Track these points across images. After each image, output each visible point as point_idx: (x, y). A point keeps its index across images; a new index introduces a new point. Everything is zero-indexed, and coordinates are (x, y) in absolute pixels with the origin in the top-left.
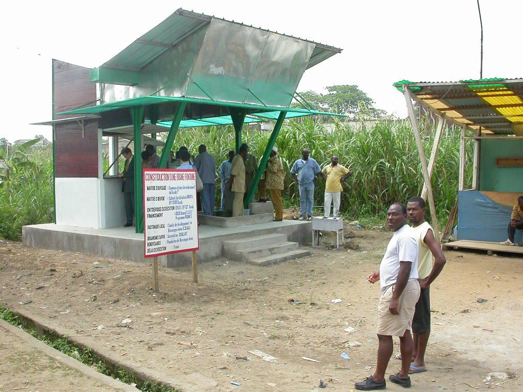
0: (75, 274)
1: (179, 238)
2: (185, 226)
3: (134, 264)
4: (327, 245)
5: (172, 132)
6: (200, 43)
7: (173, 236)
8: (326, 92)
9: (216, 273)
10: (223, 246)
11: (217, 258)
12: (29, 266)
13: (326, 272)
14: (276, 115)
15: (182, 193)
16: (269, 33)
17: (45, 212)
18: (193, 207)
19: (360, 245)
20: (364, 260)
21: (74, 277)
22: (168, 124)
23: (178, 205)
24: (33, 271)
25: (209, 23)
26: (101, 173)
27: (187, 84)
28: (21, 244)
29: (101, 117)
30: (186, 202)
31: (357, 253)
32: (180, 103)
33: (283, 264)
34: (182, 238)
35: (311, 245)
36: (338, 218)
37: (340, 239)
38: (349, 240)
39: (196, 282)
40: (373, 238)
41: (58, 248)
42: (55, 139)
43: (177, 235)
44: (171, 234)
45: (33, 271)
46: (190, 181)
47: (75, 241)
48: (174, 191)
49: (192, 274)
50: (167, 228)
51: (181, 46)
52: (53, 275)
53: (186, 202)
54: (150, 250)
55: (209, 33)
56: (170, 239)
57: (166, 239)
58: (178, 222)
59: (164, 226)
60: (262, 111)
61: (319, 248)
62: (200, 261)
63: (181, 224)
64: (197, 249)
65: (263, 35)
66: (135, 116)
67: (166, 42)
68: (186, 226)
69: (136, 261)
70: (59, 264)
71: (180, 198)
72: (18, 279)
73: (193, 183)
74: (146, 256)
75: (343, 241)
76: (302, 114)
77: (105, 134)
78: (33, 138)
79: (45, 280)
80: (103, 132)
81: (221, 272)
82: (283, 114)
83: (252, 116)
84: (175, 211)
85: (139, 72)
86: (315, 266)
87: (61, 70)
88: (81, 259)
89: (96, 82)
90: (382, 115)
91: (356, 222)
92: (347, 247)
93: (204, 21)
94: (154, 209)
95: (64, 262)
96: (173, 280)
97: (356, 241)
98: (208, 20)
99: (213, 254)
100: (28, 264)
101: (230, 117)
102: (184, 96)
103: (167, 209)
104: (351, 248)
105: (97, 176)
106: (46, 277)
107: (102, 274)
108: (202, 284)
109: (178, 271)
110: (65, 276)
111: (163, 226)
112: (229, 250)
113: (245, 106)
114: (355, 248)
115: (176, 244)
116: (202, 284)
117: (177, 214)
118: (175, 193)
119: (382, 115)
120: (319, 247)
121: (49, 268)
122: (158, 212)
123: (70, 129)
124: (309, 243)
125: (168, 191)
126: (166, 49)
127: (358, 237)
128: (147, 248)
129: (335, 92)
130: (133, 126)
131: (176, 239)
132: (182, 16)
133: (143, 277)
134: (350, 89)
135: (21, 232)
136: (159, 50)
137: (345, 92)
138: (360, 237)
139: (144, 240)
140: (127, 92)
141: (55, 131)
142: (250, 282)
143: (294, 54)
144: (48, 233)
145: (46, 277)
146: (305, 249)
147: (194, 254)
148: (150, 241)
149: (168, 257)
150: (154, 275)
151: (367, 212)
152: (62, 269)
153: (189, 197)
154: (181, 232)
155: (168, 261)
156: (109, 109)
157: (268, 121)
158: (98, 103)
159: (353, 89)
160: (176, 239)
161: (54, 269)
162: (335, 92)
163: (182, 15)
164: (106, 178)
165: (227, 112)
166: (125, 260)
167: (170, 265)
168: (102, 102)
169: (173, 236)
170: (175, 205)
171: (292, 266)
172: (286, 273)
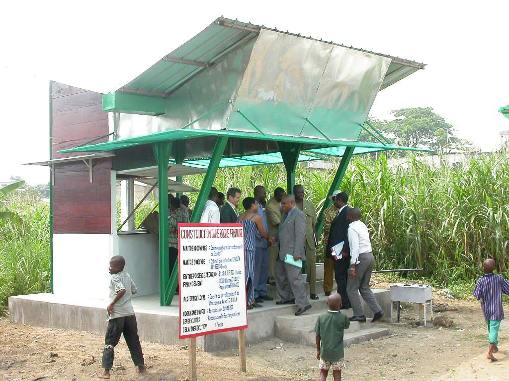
0: (84, 360)
1: (222, 312)
2: (230, 297)
3: (160, 346)
4: (410, 321)
5: (211, 172)
6: (246, 61)
7: (215, 310)
8: (391, 118)
9: (268, 358)
10: (275, 323)
11: (268, 338)
12: (22, 349)
13: (413, 357)
14: (341, 151)
15: (227, 254)
16: (332, 45)
17: (37, 278)
18: (240, 272)
19: (454, 320)
20: (462, 342)
21: (83, 365)
22: (204, 164)
23: (222, 270)
24: (28, 356)
25: (258, 34)
26: (114, 229)
27: (228, 113)
28: (7, 320)
29: (115, 155)
30: (231, 266)
31: (452, 332)
32: (220, 137)
33: (354, 347)
34: (227, 312)
35: (388, 322)
36: (424, 286)
37: (428, 312)
38: (439, 314)
39: (244, 370)
40: (471, 311)
41: (56, 325)
42: (53, 184)
43: (220, 310)
44: (213, 307)
45: (28, 356)
46: (236, 238)
47: (79, 316)
48: (216, 251)
49: (238, 360)
50: (207, 300)
51: (221, 64)
52: (54, 361)
53: (231, 266)
54: (187, 328)
55: (259, 47)
56: (212, 315)
57: (207, 314)
58: (221, 292)
59: (204, 296)
60: (321, 146)
61: (400, 326)
62: (247, 344)
63: (225, 296)
64: (246, 327)
65: (325, 49)
66: (159, 153)
67: (202, 59)
68: (232, 297)
69: (162, 343)
70: (61, 347)
71: (224, 260)
72: (9, 367)
73: (240, 241)
74: (182, 337)
75: (433, 316)
76: (377, 149)
77: (120, 177)
78: (9, 182)
79: (44, 368)
80: (117, 175)
81: (274, 358)
82: (349, 150)
83: (307, 153)
84: (218, 277)
85: (165, 98)
86: (397, 350)
87: (61, 94)
88: (89, 340)
89: (109, 111)
90: (467, 146)
91: (447, 290)
92: (438, 323)
93: (251, 32)
94: (191, 276)
95: (67, 344)
96: (215, 368)
97: (450, 315)
98: (256, 31)
99: (262, 334)
100: (20, 348)
101: (279, 154)
102: (225, 129)
103: (208, 275)
104: (444, 326)
105: (108, 231)
106: (46, 364)
107: (120, 360)
108: (253, 374)
109: (218, 356)
110: (70, 363)
111: (202, 298)
112: (284, 328)
113: (301, 140)
114: (448, 325)
115: (219, 321)
116: (253, 374)
117: (220, 281)
118: (219, 254)
119: (467, 146)
120: (401, 323)
121: (49, 353)
122: (196, 280)
123: (74, 171)
124: (386, 319)
125: (209, 251)
126: (202, 68)
127: (451, 310)
128: (183, 326)
129: (403, 117)
130: (157, 167)
131: (219, 314)
132: (223, 27)
133: (176, 364)
134: (423, 113)
135: (7, 305)
136: (193, 69)
137: (416, 117)
138: (454, 311)
139: (179, 316)
140: (150, 123)
141: (53, 172)
142: (313, 371)
143: (364, 74)
144: (44, 306)
145: (46, 364)
146: (382, 327)
147: (241, 333)
148: (186, 318)
149: (205, 338)
150: (191, 362)
151: (460, 276)
152: (66, 354)
153: (235, 259)
154: (225, 305)
155: (205, 343)
156: (125, 145)
157: (326, 158)
158: (111, 138)
159: (427, 113)
160: (219, 314)
161: (55, 353)
162: (403, 117)
163: (223, 25)
164: (121, 234)
165: (276, 149)
166: (148, 341)
167: (208, 349)
168: (116, 136)
169: (215, 310)
170: (218, 270)
171: (367, 349)
172: (360, 359)
